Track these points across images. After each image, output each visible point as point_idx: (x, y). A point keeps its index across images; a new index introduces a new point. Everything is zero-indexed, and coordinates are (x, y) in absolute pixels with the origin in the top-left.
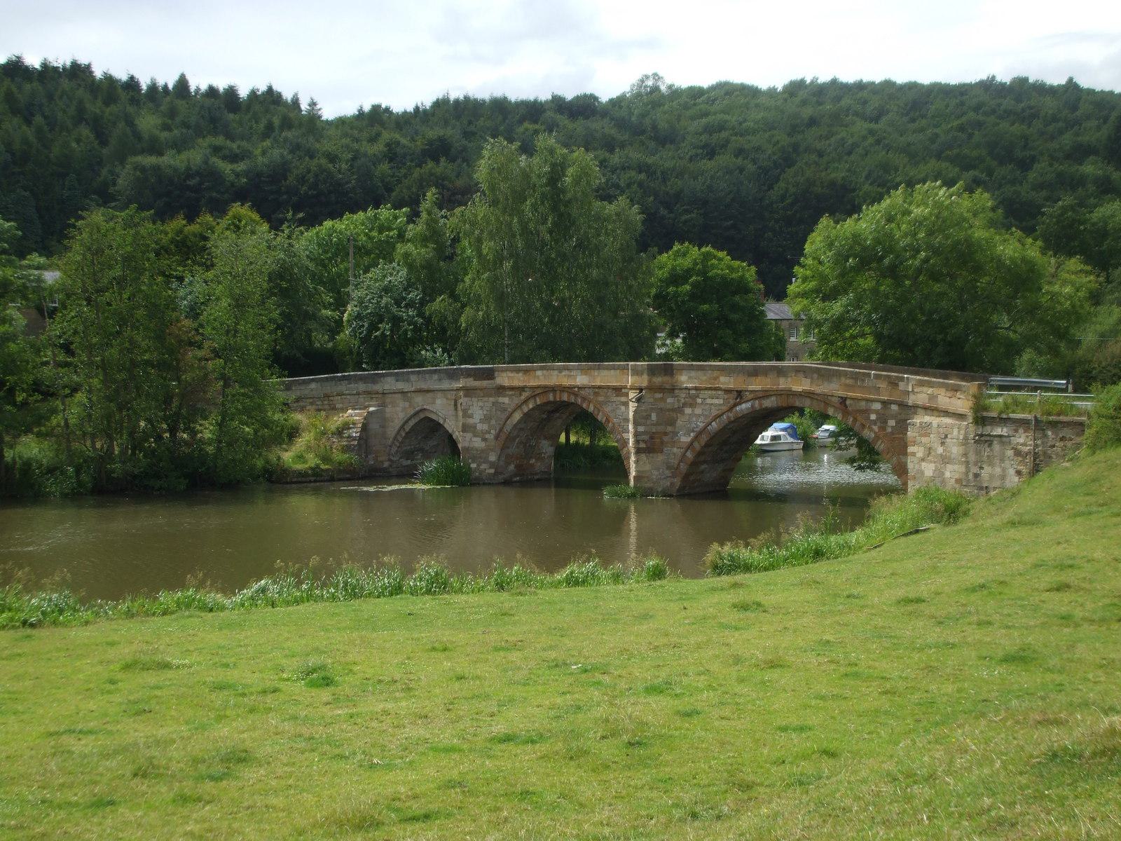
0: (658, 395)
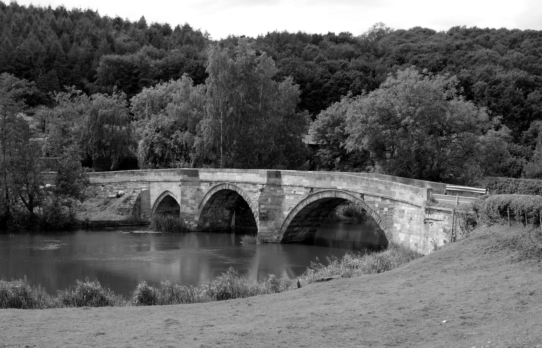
0: (272, 188)
